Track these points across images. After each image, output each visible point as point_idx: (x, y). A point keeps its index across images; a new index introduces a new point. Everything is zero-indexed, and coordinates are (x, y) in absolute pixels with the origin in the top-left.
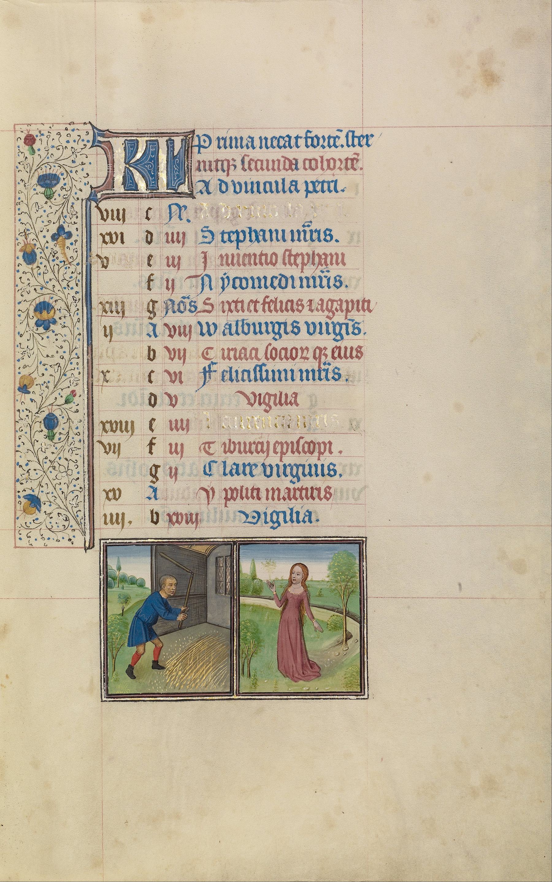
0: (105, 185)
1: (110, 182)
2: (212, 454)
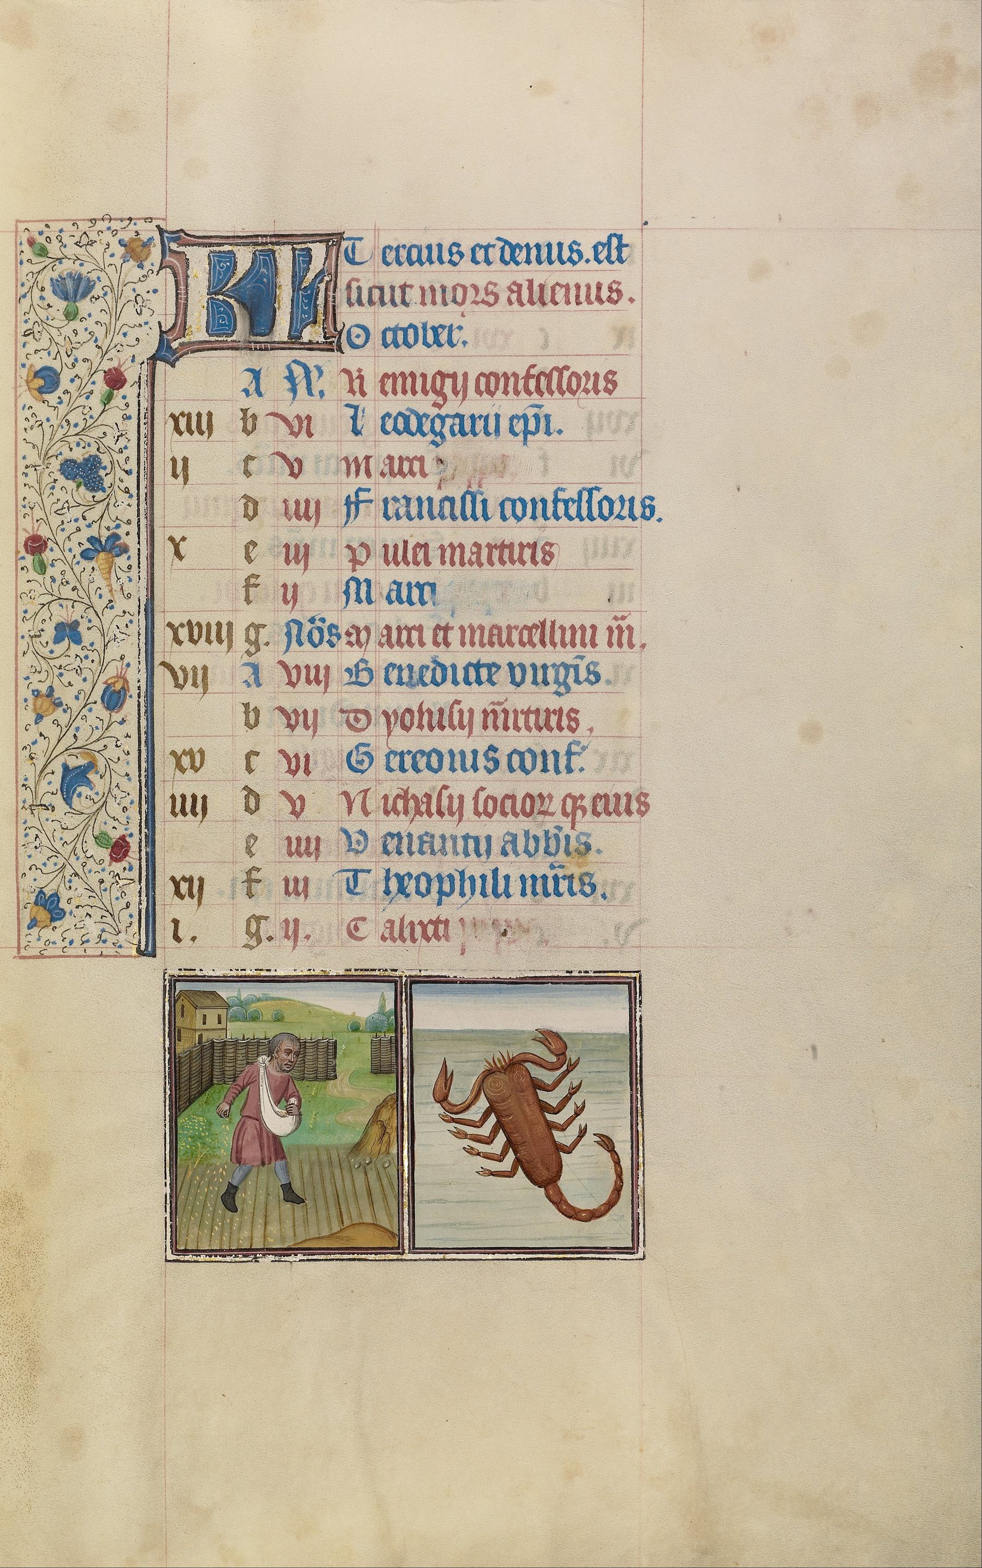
0: (189, 238)
1: (181, 325)
2: (361, 939)
